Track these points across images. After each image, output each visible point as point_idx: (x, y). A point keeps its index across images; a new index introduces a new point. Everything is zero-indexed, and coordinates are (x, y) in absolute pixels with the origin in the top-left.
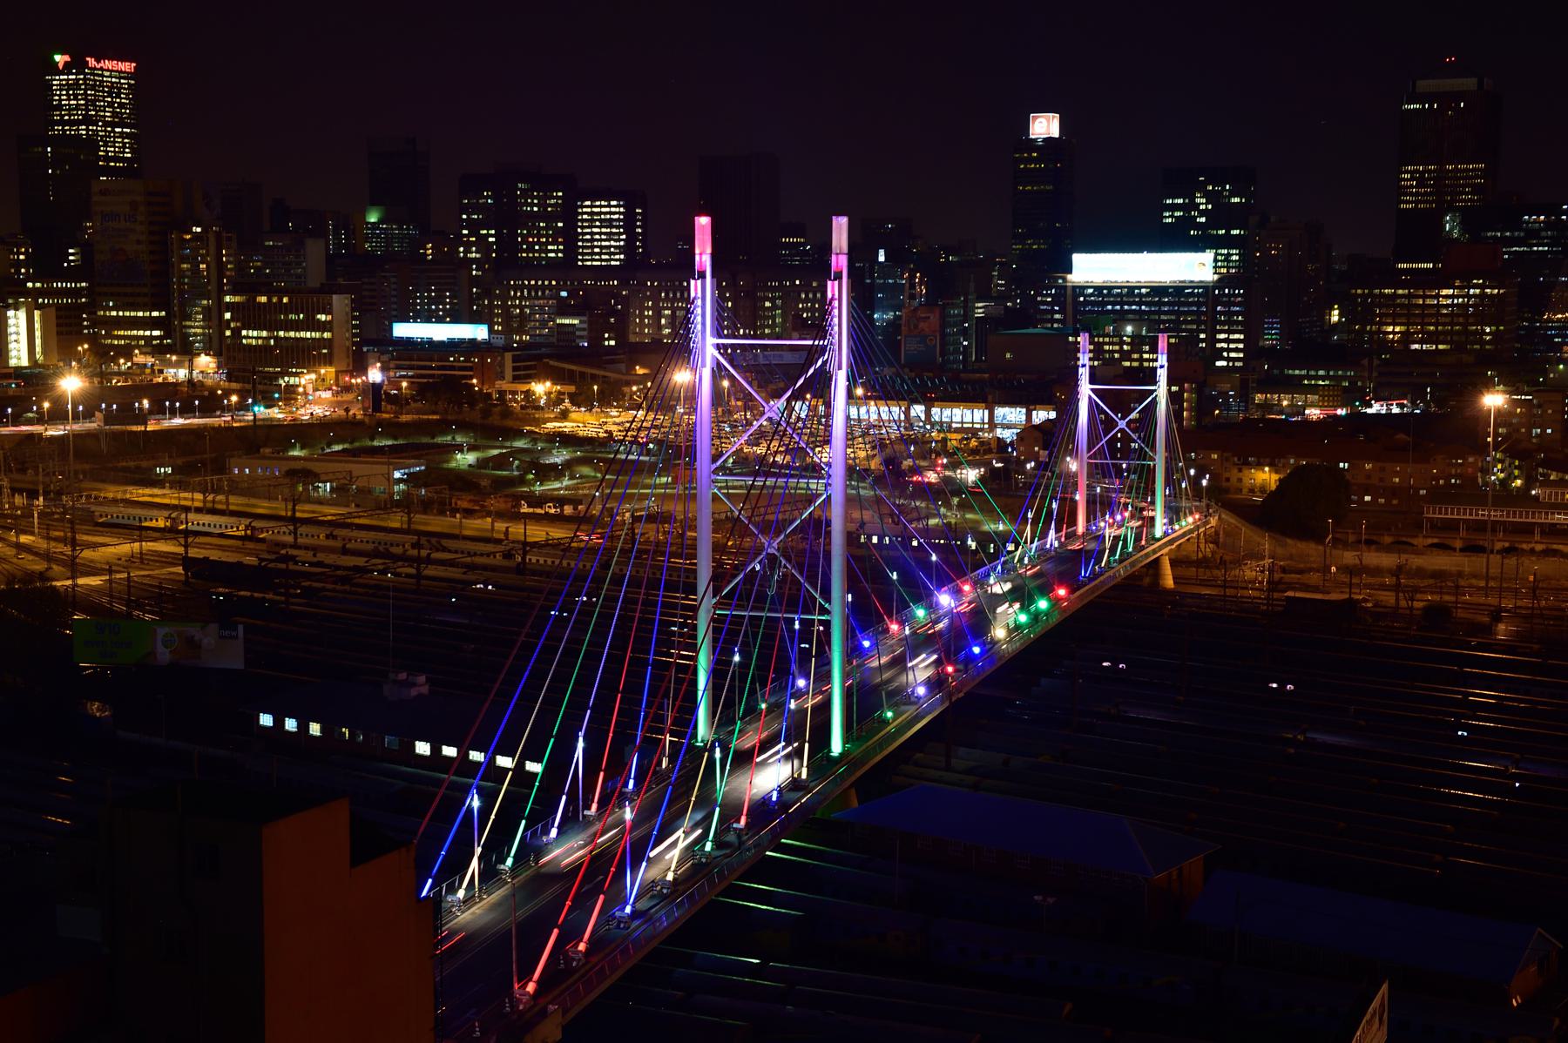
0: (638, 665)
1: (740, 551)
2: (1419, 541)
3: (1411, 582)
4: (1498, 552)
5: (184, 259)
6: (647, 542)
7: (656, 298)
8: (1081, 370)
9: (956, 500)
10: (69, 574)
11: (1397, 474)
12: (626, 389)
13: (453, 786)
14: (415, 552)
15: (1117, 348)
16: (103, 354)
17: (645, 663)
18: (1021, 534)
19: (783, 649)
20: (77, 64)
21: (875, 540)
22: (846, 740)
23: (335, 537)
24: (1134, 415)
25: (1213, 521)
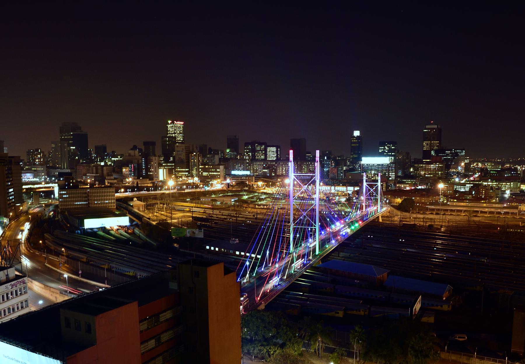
0: (279, 237)
1: (298, 215)
2: (428, 213)
3: (426, 220)
4: (442, 214)
5: (192, 159)
6: (281, 213)
7: (282, 166)
8: (364, 180)
9: (340, 205)
10: (171, 219)
11: (423, 200)
12: (276, 184)
13: (243, 260)
14: (236, 215)
15: (371, 176)
16: (177, 177)
17: (280, 237)
18: (353, 211)
19: (307, 234)
20: (173, 123)
21: (324, 213)
22: (319, 251)
23: (220, 212)
24: (374, 189)
25: (389, 209)
